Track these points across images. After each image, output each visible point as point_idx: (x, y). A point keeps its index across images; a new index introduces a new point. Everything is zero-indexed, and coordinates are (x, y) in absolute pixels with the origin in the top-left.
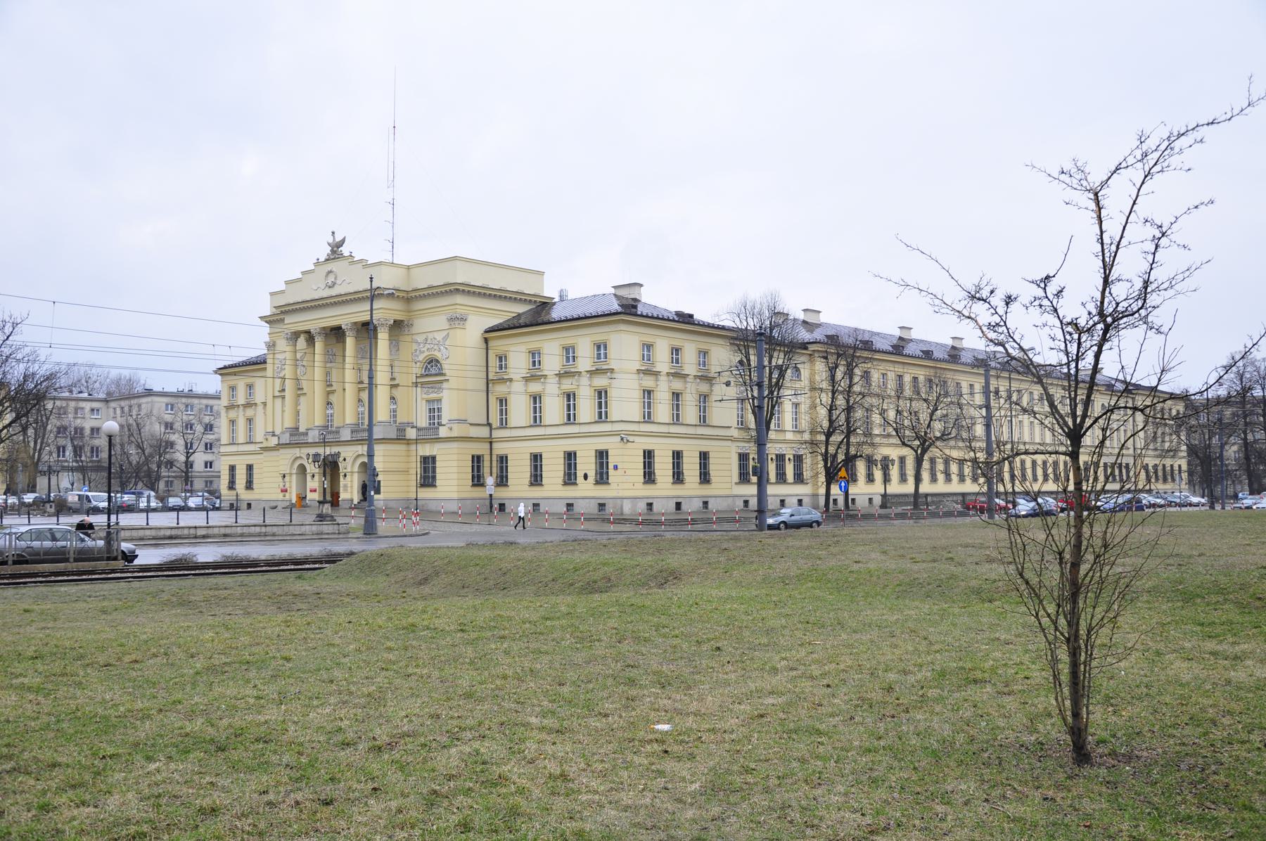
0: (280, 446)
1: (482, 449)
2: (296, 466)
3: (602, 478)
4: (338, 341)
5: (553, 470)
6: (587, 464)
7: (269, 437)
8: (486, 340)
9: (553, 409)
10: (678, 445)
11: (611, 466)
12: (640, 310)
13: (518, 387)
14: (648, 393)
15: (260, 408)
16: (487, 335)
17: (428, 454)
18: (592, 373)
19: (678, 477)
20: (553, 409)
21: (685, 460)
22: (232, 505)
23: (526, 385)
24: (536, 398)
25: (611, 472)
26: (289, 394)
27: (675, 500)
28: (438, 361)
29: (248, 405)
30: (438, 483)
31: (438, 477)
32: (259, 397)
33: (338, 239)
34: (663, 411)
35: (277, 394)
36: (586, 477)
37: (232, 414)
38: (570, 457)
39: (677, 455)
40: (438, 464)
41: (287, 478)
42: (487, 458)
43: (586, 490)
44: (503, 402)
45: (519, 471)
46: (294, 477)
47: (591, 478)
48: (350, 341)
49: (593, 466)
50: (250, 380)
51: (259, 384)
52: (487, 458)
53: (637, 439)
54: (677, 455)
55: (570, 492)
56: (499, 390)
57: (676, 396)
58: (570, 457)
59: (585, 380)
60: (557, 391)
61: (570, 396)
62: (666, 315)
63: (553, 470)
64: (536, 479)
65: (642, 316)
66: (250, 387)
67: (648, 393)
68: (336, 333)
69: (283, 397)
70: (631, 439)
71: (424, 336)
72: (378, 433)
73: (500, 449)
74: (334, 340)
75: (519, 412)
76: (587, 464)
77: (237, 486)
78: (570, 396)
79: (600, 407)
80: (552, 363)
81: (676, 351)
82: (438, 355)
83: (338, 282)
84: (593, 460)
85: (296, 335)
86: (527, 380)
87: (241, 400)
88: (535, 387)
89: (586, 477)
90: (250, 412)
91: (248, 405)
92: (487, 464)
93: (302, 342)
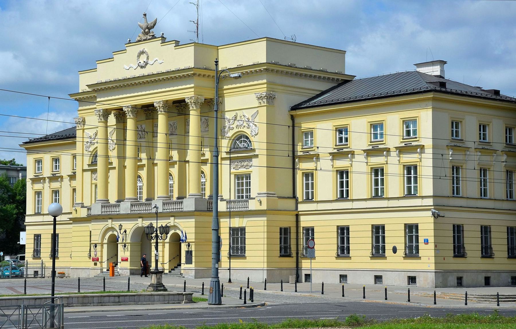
0: (90, 218)
1: (288, 221)
2: (107, 237)
3: (286, 251)
4: (180, 114)
5: (361, 242)
6: (395, 237)
7: (79, 208)
8: (293, 118)
9: (360, 185)
10: (486, 219)
11: (421, 240)
12: (449, 87)
13: (360, 158)
14: (456, 169)
15: (66, 180)
16: (294, 113)
17: (237, 226)
18: (401, 150)
19: (487, 252)
20: (360, 185)
21: (466, 234)
22: (36, 273)
23: (332, 160)
24: (343, 173)
25: (421, 246)
26: (100, 166)
27: (484, 275)
28: (247, 138)
29: (54, 178)
30: (247, 254)
31: (247, 247)
32: (65, 170)
33: (150, 22)
34: (470, 187)
35: (86, 167)
36: (395, 250)
37: (38, 187)
38: (378, 231)
39: (485, 231)
40: (247, 236)
41: (99, 247)
42: (293, 230)
43: (395, 264)
44: (308, 175)
45: (326, 243)
46: (105, 246)
47: (401, 252)
48: (161, 119)
49: (403, 240)
50: (55, 155)
51: (66, 158)
52: (293, 230)
53: (447, 214)
54: (485, 231)
55: (378, 265)
56: (304, 166)
57: (483, 171)
58: (378, 231)
59: (47, 184)
60: (366, 169)
61: (378, 172)
62: (469, 91)
63: (361, 242)
64: (344, 250)
65: (451, 93)
66: (56, 160)
67: (456, 169)
68: (148, 111)
69: (94, 171)
70: (442, 213)
71: (234, 113)
72: (222, 207)
73: (305, 221)
74: (143, 117)
75: (326, 186)
76: (395, 237)
77: (42, 255)
78: (378, 172)
79: (342, 186)
80: (359, 137)
81: (483, 127)
82: (248, 132)
83: (150, 62)
84: (402, 233)
85: (106, 114)
86: (334, 156)
87: (47, 172)
88: (342, 164)
89: (395, 250)
90: (55, 185)
91: (54, 178)
92: (293, 235)
93: (112, 120)
